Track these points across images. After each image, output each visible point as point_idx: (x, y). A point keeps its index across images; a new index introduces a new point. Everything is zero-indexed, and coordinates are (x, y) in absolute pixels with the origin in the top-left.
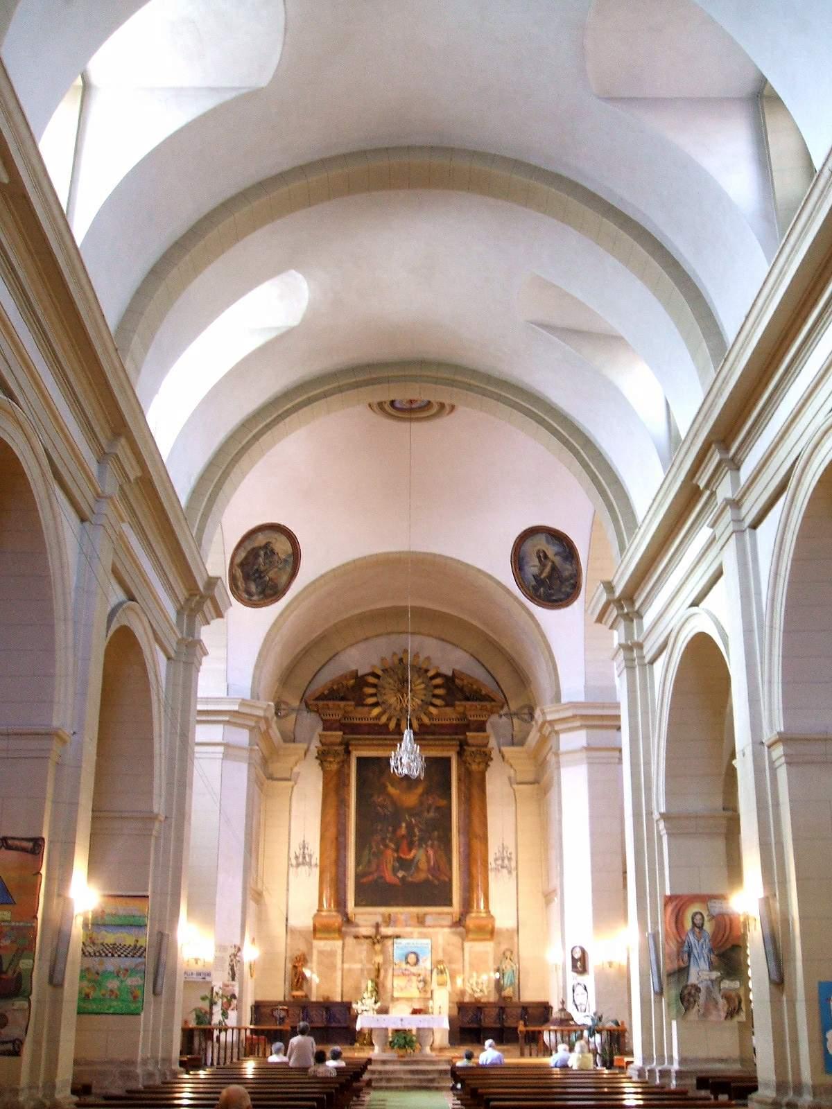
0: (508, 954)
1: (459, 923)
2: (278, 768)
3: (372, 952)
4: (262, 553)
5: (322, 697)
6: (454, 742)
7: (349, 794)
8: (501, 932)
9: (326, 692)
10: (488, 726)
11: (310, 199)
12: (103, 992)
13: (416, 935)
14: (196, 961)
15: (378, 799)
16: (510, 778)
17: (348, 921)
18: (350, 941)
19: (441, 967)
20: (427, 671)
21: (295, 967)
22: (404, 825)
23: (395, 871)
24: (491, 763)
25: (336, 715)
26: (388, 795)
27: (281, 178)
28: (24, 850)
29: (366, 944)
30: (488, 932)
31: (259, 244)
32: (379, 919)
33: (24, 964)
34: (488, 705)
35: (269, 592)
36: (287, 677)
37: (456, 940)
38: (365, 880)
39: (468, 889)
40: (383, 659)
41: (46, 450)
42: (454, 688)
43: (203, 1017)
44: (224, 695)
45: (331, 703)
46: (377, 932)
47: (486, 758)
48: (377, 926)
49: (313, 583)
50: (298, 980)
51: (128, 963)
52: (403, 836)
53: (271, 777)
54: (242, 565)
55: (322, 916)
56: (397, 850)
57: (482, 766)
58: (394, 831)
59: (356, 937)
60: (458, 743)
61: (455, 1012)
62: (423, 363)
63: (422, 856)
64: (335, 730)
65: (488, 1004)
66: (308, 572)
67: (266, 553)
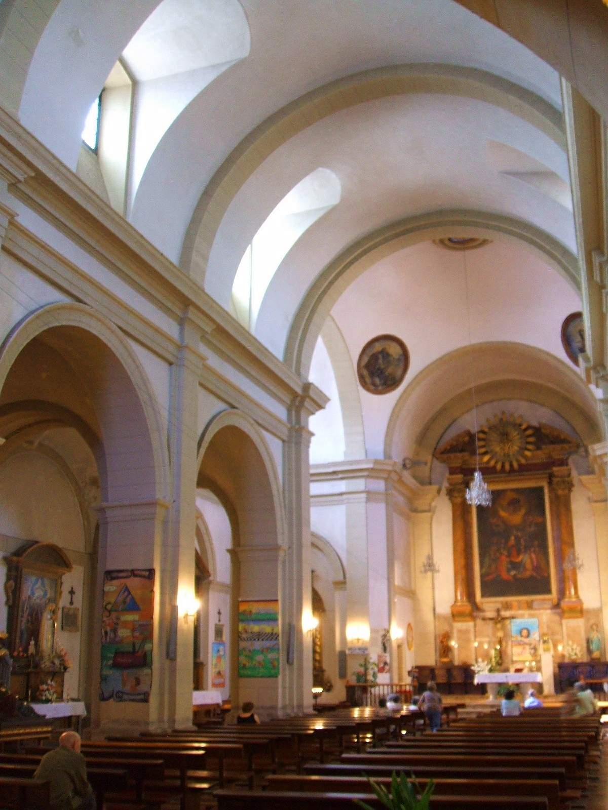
0: (594, 627)
1: (557, 606)
2: (421, 503)
3: (495, 630)
4: (380, 356)
5: (442, 453)
6: (544, 476)
7: (472, 519)
8: (588, 611)
9: (448, 448)
10: (570, 461)
11: (308, 121)
12: (254, 662)
13: (526, 616)
14: (358, 640)
15: (494, 521)
16: (589, 499)
17: (476, 608)
18: (479, 622)
19: (545, 638)
20: (520, 425)
21: (442, 642)
22: (513, 538)
23: (508, 570)
24: (573, 489)
25: (457, 463)
26: (500, 517)
27: (282, 112)
28: (144, 577)
29: (491, 623)
30: (578, 611)
31: (283, 156)
32: (499, 606)
33: (147, 647)
34: (566, 446)
35: (389, 383)
36: (421, 439)
37: (557, 618)
38: (487, 579)
39: (562, 581)
40: (488, 420)
41: (120, 328)
42: (541, 436)
43: (362, 677)
44: (363, 457)
45: (452, 455)
46: (499, 615)
47: (570, 486)
48: (498, 611)
49: (421, 372)
50: (445, 650)
51: (268, 644)
52: (513, 546)
53: (415, 511)
54: (367, 366)
55: (457, 606)
56: (509, 556)
57: (567, 491)
58: (507, 542)
59: (484, 619)
60: (547, 475)
61: (557, 670)
62: (441, 212)
63: (527, 559)
64: (457, 474)
65: (582, 664)
66: (416, 365)
67: (383, 356)
